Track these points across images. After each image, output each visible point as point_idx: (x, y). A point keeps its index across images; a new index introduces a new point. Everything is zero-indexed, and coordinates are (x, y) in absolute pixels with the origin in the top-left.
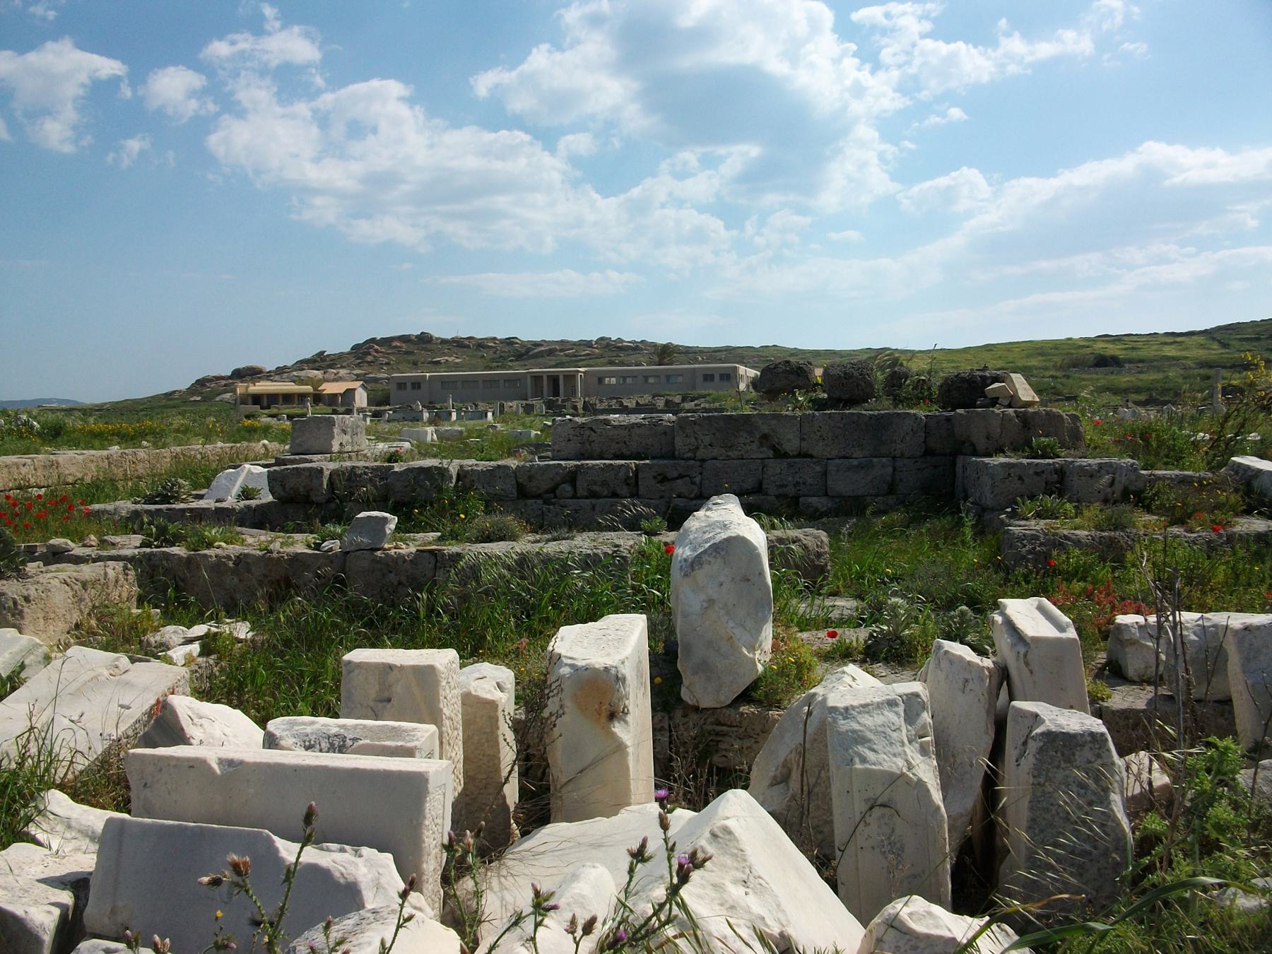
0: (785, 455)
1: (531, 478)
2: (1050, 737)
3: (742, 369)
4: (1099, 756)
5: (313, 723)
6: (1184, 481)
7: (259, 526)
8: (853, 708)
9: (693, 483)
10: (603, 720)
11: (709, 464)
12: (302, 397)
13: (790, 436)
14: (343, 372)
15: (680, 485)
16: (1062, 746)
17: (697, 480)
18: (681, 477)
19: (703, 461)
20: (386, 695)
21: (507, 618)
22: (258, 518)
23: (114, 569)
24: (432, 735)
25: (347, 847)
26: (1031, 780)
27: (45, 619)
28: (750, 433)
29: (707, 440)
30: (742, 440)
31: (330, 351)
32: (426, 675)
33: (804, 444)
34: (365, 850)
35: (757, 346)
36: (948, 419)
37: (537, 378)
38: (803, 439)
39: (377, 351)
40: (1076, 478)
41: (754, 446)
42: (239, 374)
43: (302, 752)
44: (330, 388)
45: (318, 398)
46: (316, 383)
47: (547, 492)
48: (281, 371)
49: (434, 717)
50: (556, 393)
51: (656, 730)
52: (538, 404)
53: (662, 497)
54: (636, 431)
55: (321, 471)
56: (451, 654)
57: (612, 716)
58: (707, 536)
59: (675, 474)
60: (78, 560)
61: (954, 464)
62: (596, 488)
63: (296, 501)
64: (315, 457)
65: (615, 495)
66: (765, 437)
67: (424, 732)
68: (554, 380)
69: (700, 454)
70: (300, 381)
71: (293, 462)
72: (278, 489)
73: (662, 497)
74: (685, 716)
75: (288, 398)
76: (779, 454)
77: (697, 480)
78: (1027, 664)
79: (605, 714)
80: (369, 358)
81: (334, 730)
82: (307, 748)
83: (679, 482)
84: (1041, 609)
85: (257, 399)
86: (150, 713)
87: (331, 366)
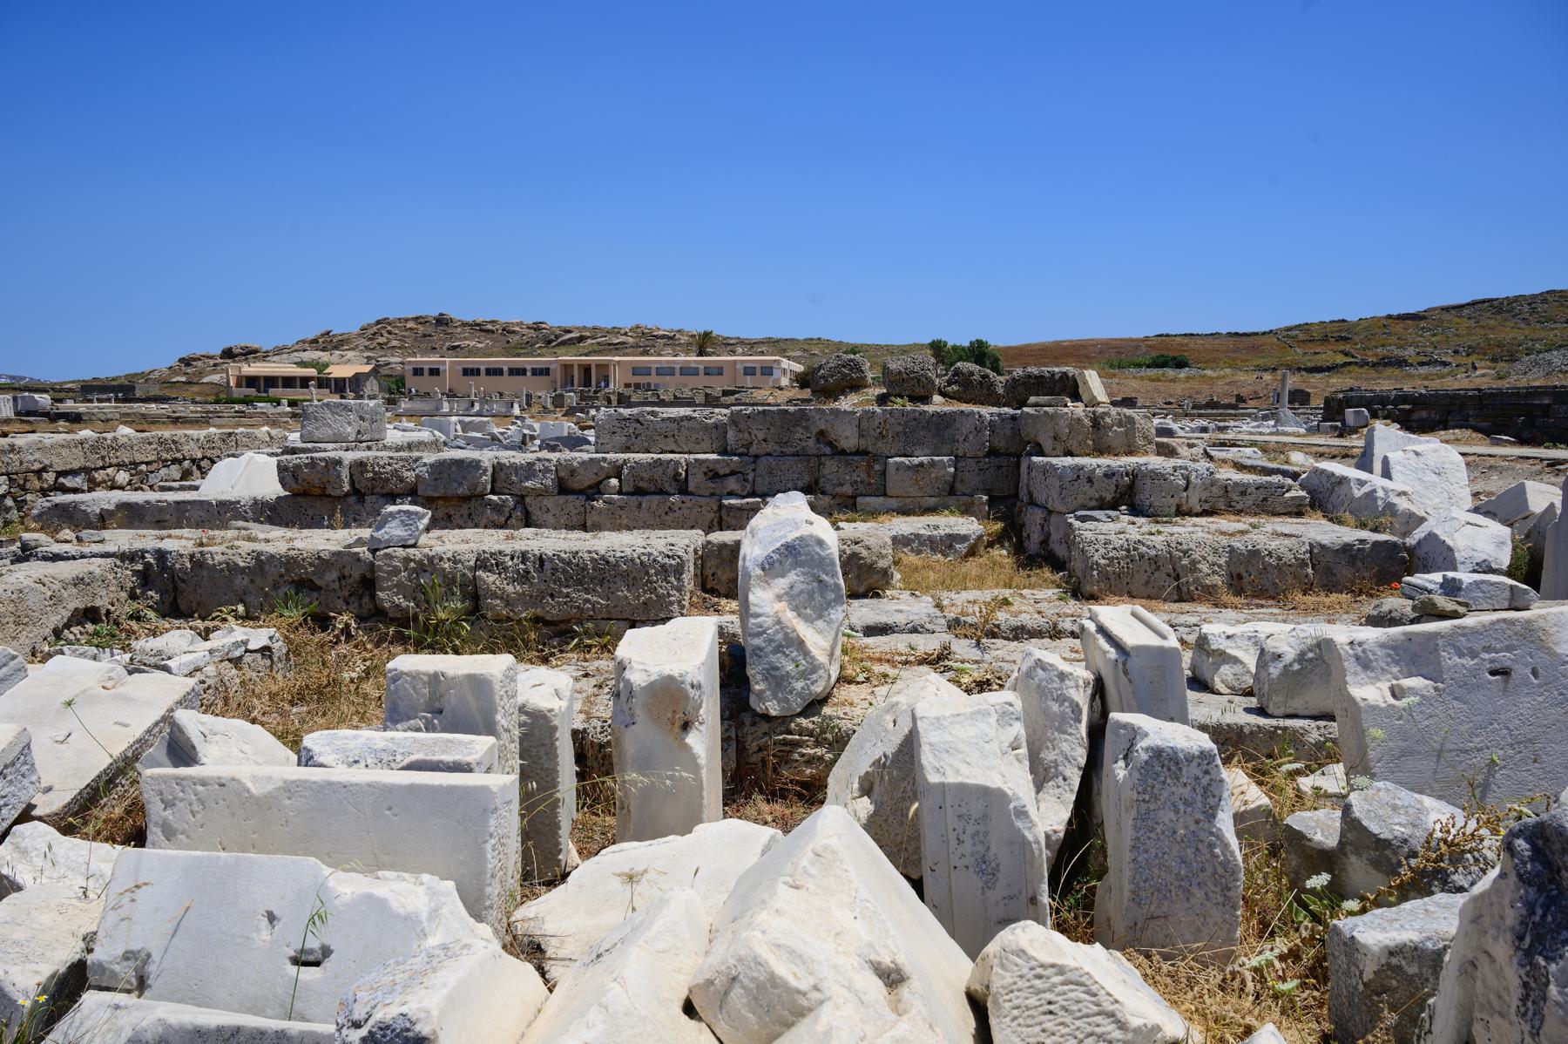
0: (843, 452)
1: (573, 472)
2: (1157, 753)
3: (785, 363)
4: (1207, 772)
5: (356, 737)
6: (587, 591)
7: (272, 521)
8: (945, 718)
9: (746, 480)
10: (677, 729)
11: (763, 462)
12: (305, 382)
14: (350, 354)
16: (1164, 759)
18: (733, 473)
19: (757, 457)
20: (437, 705)
21: (569, 616)
22: (269, 512)
23: (96, 566)
24: (492, 747)
25: (406, 875)
26: (1135, 796)
27: (17, 624)
28: (807, 428)
29: (761, 435)
30: (797, 436)
31: (336, 331)
32: (478, 684)
33: (862, 442)
34: (426, 877)
35: (801, 338)
36: (1013, 418)
37: (567, 367)
38: (861, 436)
39: (390, 333)
40: (1148, 482)
41: (811, 443)
42: (228, 354)
43: (342, 768)
44: (337, 371)
45: (323, 383)
46: (321, 366)
47: (590, 487)
48: (279, 351)
49: (490, 729)
50: (587, 383)
51: (725, 740)
52: (572, 398)
53: (713, 494)
54: (685, 423)
55: (339, 462)
56: (506, 659)
57: (686, 726)
58: (777, 534)
59: (727, 471)
60: (56, 558)
61: (1018, 465)
62: (642, 484)
63: (308, 495)
64: (330, 446)
65: (661, 492)
66: (822, 433)
67: (477, 746)
68: (586, 370)
69: (754, 450)
70: (302, 364)
71: (304, 451)
72: (289, 480)
73: (713, 494)
74: (754, 724)
75: (288, 382)
76: (840, 453)
78: (1126, 673)
79: (678, 724)
80: (381, 340)
81: (380, 745)
82: (350, 765)
83: (732, 479)
84: (1134, 614)
85: (251, 381)
86: (1407, 900)
87: (336, 348)
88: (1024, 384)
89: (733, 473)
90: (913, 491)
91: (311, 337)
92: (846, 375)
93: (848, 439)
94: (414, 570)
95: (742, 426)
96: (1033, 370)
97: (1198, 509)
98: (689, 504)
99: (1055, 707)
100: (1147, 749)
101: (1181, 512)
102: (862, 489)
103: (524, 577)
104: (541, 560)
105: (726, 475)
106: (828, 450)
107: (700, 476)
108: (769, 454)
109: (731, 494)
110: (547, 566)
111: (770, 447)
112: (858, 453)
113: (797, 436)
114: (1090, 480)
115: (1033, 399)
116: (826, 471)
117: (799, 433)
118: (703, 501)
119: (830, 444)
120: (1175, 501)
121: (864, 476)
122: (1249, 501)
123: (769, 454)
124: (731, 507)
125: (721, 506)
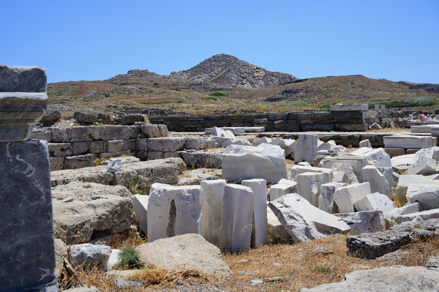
9: (71, 151)
11: (76, 144)
13: (97, 134)
15: (68, 152)
17: (72, 149)
18: (68, 148)
19: (72, 143)
28: (86, 133)
29: (74, 136)
30: (84, 135)
53: (62, 156)
69: (72, 141)
73: (62, 156)
76: (94, 140)
77: (72, 149)
83: (68, 151)
88: (129, 118)
89: (68, 148)
90: (115, 150)
91: (267, 70)
92: (56, 116)
93: (97, 136)
94: (125, 177)
95: (69, 133)
96: (132, 115)
97: (203, 148)
98: (55, 160)
99: (349, 171)
100: (135, 197)
101: (200, 149)
102: (102, 151)
103: (149, 175)
104: (152, 170)
105: (66, 149)
106: (91, 139)
107: (59, 150)
108: (76, 142)
109: (68, 155)
110: (153, 171)
111: (77, 139)
112: (99, 140)
113: (84, 135)
114: (178, 143)
115: (136, 123)
116: (92, 146)
117: (84, 135)
118: (59, 158)
119: (92, 138)
120: (199, 146)
121: (102, 147)
122: (211, 145)
123: (76, 142)
124: (69, 160)
125: (65, 159)
